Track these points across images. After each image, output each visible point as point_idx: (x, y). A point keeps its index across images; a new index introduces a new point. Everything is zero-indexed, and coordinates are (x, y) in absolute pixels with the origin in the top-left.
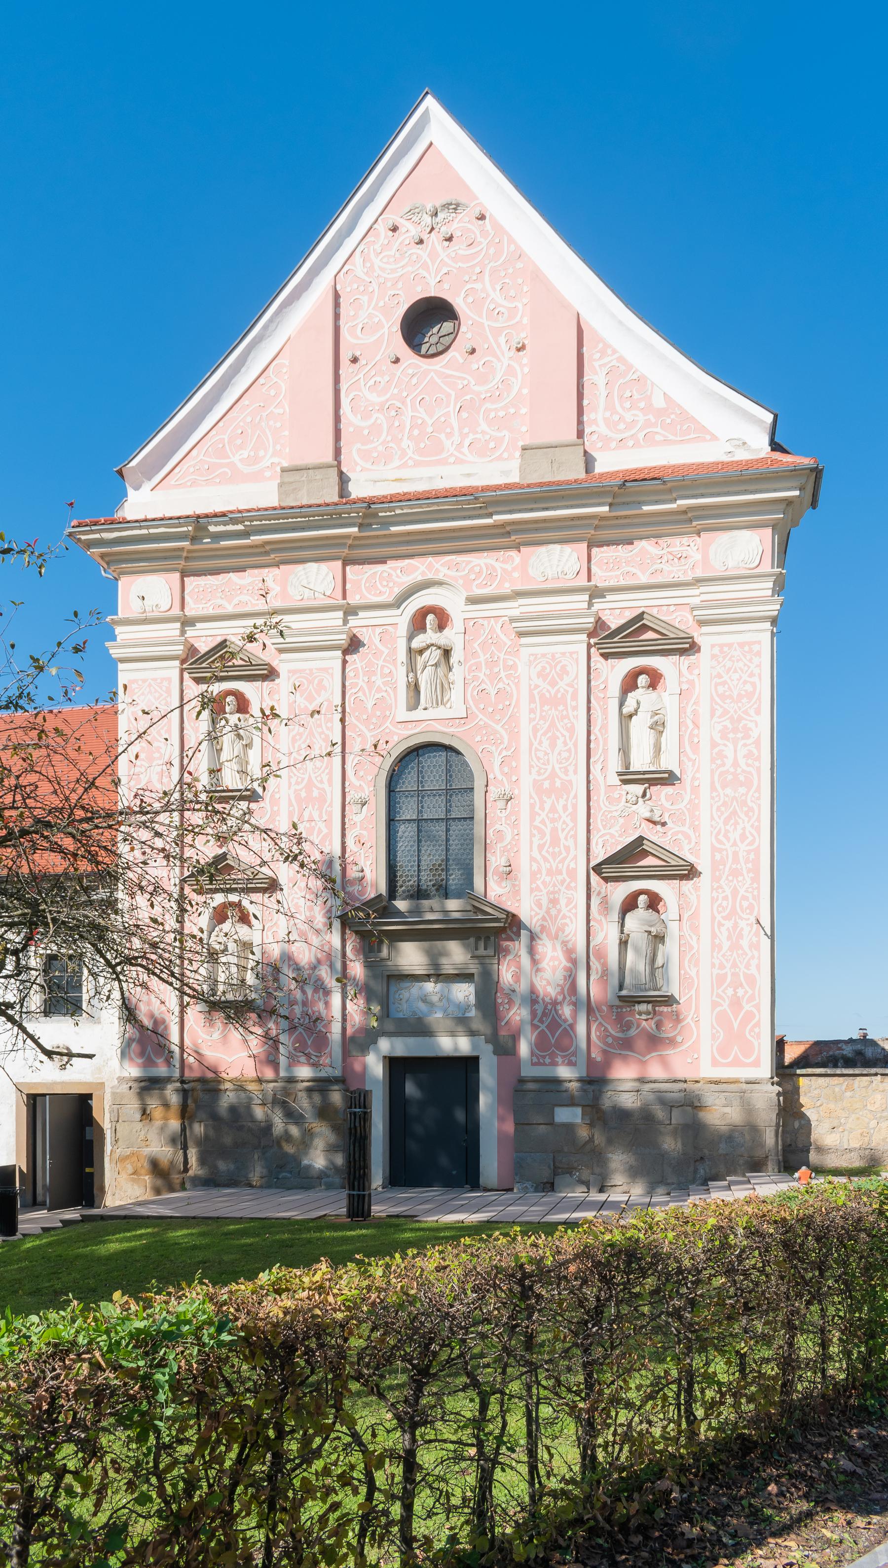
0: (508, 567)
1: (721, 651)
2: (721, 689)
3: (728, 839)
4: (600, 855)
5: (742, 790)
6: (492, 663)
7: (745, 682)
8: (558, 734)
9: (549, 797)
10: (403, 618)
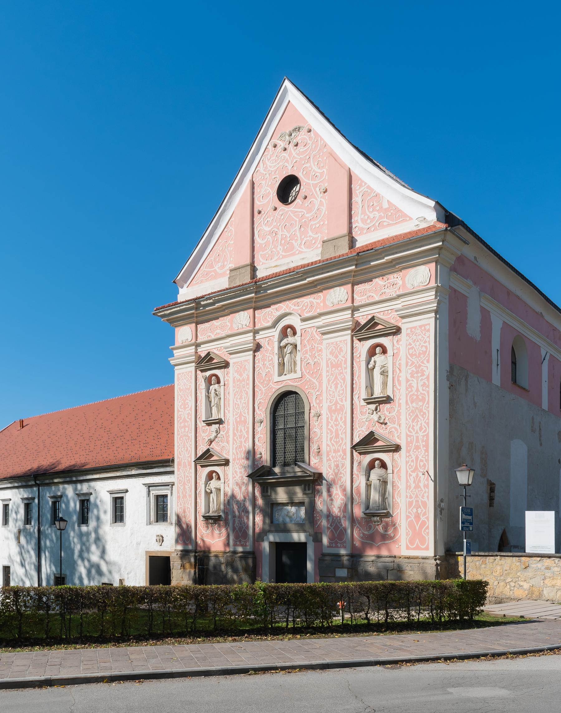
0: (319, 301)
1: (411, 331)
2: (411, 351)
3: (414, 430)
4: (357, 440)
5: (420, 404)
6: (312, 349)
7: (422, 346)
8: (338, 382)
9: (335, 414)
10: (276, 333)
